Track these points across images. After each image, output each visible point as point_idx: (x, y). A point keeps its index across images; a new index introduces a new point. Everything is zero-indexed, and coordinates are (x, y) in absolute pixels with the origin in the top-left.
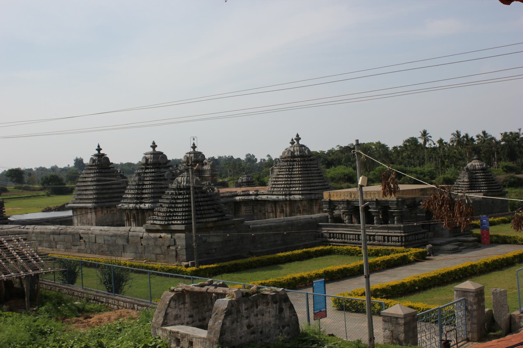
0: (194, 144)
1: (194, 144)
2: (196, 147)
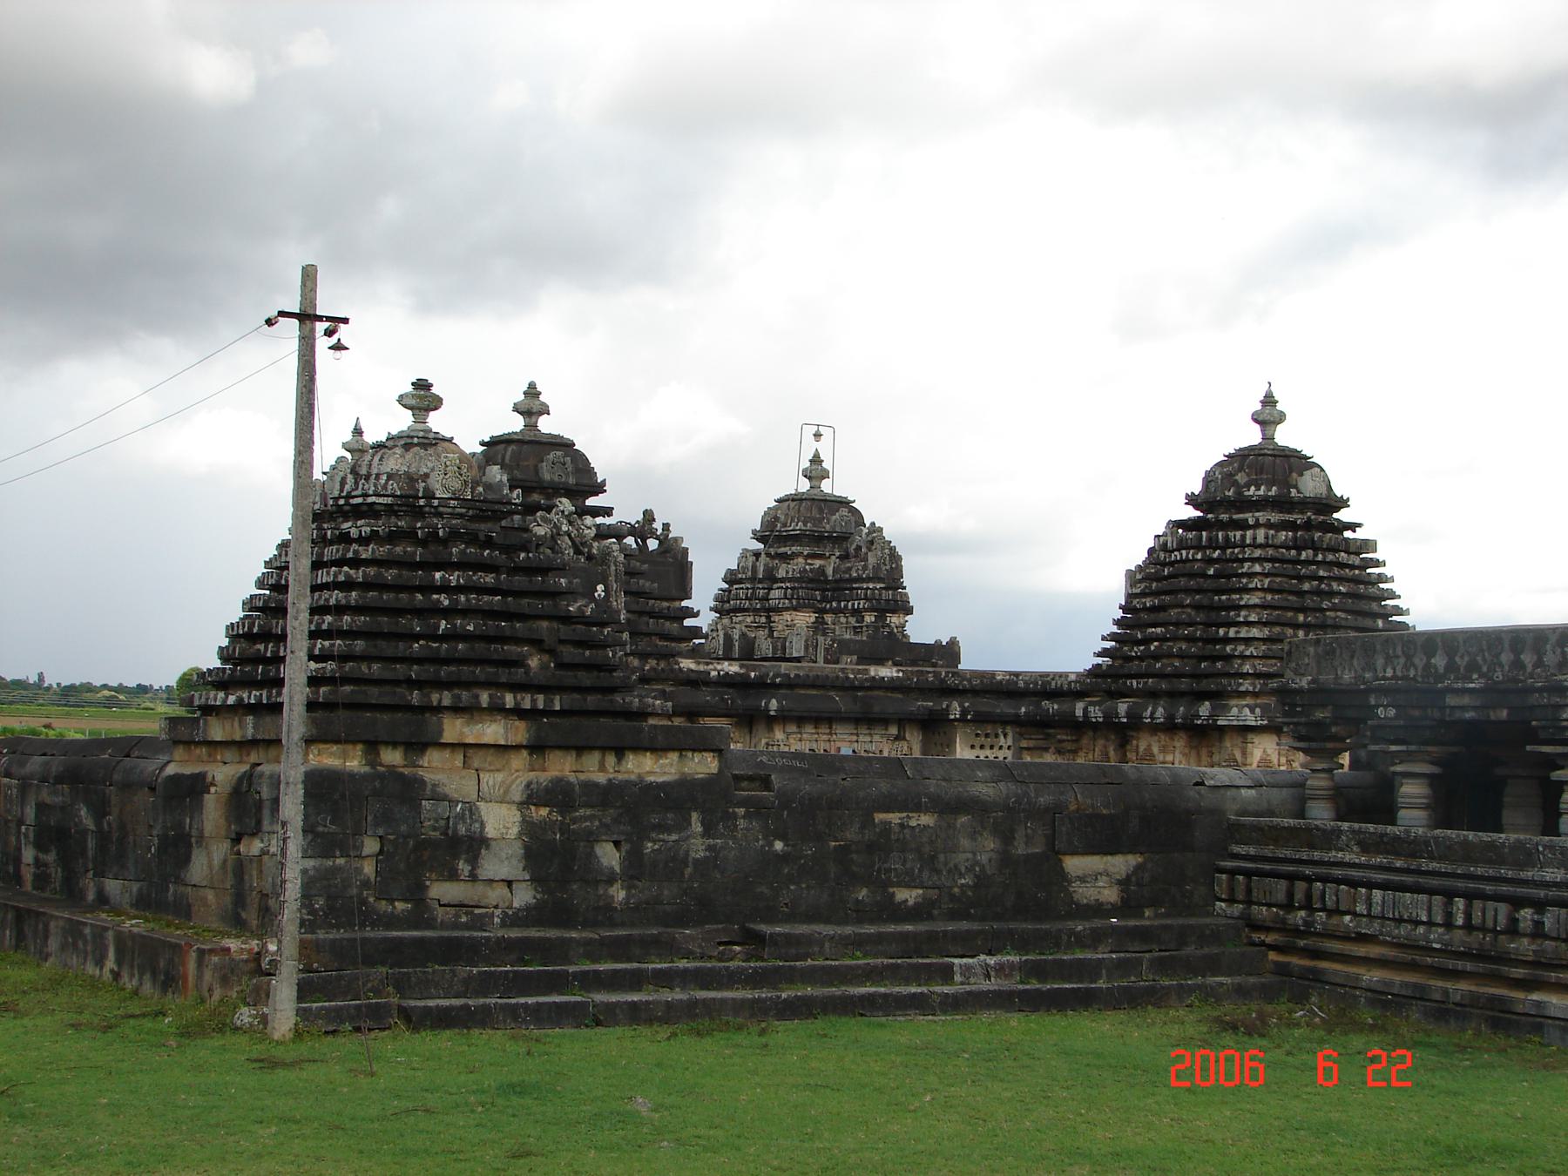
0: (816, 460)
1: (816, 460)
2: (825, 475)
